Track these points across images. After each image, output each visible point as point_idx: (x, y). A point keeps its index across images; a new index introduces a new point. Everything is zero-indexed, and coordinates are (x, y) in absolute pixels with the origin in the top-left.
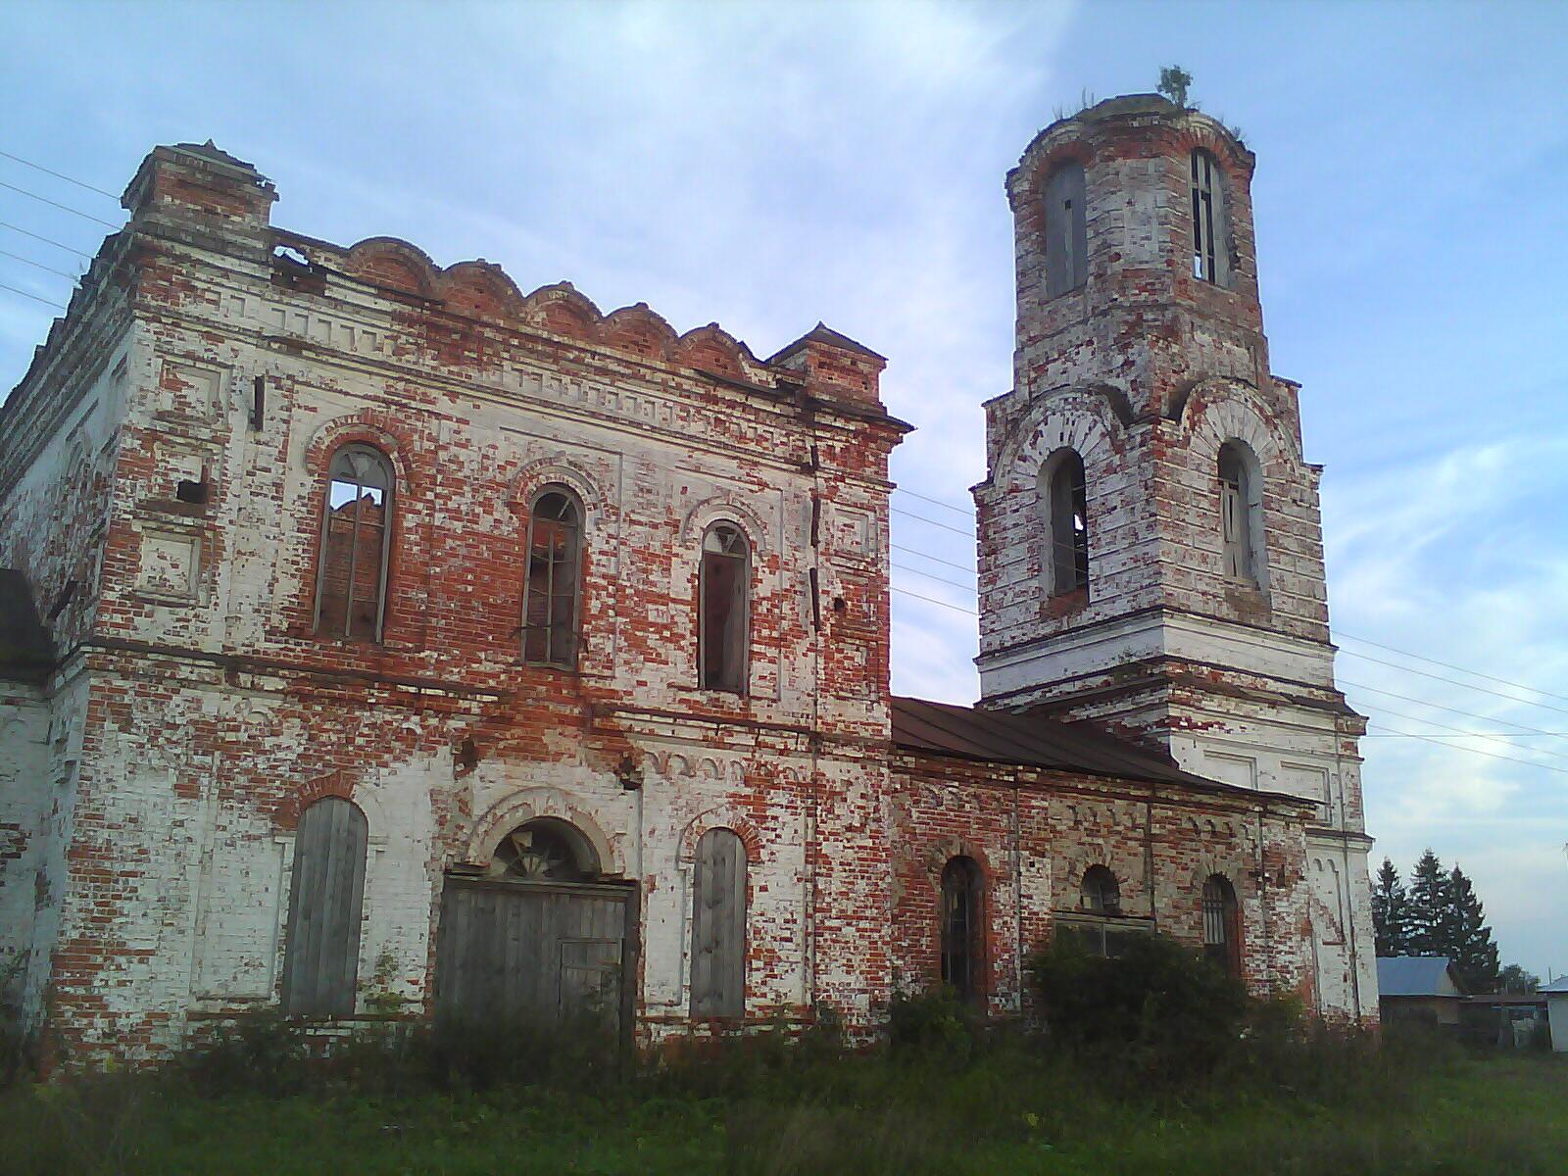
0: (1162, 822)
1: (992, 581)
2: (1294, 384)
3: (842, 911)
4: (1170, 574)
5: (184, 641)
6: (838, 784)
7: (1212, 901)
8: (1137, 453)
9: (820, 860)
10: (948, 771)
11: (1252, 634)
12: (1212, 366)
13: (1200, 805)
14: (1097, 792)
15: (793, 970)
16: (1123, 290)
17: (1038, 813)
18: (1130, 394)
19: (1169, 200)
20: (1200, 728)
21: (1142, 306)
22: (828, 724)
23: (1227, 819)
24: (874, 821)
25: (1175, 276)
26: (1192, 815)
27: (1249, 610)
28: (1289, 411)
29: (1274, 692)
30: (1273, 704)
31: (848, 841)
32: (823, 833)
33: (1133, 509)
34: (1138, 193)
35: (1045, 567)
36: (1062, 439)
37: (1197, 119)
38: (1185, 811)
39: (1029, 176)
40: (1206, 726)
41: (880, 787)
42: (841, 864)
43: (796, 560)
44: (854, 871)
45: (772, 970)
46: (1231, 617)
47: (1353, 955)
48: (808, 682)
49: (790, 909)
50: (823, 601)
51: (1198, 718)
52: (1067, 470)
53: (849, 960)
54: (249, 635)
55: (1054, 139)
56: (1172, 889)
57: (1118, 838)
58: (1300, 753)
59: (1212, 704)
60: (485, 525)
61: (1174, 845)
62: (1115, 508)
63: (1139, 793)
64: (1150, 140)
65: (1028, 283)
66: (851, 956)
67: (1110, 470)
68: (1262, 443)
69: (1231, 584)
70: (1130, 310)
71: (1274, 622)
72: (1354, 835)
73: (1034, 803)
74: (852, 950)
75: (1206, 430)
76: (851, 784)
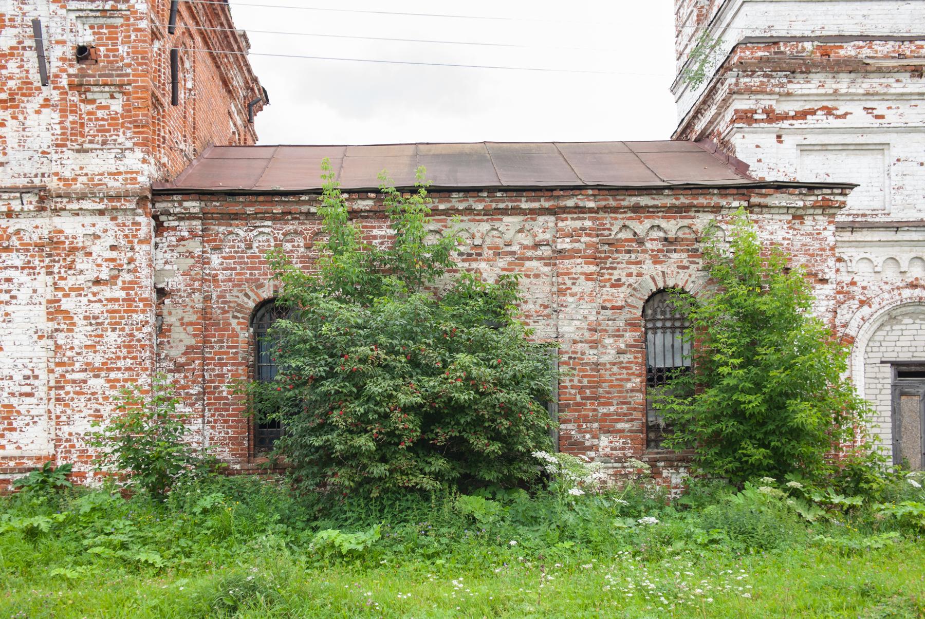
3: (87, 364)
6: (80, 240)
7: (673, 319)
9: (60, 317)
10: (250, 210)
13: (636, 209)
14: (469, 211)
15: (35, 422)
17: (382, 243)
20: (793, 118)
22: (66, 180)
23: (686, 222)
24: (129, 271)
26: (628, 223)
31: (94, 294)
32: (63, 289)
38: (616, 219)
40: (802, 115)
41: (135, 236)
42: (86, 318)
43: (24, 14)
44: (102, 324)
45: (10, 424)
48: (45, 140)
49: (30, 366)
50: (55, 54)
51: (782, 107)
53: (97, 410)
59: (808, 87)
61: (595, 259)
63: (535, 205)
66: (99, 407)
73: (376, 232)
74: (101, 400)
76: (99, 237)
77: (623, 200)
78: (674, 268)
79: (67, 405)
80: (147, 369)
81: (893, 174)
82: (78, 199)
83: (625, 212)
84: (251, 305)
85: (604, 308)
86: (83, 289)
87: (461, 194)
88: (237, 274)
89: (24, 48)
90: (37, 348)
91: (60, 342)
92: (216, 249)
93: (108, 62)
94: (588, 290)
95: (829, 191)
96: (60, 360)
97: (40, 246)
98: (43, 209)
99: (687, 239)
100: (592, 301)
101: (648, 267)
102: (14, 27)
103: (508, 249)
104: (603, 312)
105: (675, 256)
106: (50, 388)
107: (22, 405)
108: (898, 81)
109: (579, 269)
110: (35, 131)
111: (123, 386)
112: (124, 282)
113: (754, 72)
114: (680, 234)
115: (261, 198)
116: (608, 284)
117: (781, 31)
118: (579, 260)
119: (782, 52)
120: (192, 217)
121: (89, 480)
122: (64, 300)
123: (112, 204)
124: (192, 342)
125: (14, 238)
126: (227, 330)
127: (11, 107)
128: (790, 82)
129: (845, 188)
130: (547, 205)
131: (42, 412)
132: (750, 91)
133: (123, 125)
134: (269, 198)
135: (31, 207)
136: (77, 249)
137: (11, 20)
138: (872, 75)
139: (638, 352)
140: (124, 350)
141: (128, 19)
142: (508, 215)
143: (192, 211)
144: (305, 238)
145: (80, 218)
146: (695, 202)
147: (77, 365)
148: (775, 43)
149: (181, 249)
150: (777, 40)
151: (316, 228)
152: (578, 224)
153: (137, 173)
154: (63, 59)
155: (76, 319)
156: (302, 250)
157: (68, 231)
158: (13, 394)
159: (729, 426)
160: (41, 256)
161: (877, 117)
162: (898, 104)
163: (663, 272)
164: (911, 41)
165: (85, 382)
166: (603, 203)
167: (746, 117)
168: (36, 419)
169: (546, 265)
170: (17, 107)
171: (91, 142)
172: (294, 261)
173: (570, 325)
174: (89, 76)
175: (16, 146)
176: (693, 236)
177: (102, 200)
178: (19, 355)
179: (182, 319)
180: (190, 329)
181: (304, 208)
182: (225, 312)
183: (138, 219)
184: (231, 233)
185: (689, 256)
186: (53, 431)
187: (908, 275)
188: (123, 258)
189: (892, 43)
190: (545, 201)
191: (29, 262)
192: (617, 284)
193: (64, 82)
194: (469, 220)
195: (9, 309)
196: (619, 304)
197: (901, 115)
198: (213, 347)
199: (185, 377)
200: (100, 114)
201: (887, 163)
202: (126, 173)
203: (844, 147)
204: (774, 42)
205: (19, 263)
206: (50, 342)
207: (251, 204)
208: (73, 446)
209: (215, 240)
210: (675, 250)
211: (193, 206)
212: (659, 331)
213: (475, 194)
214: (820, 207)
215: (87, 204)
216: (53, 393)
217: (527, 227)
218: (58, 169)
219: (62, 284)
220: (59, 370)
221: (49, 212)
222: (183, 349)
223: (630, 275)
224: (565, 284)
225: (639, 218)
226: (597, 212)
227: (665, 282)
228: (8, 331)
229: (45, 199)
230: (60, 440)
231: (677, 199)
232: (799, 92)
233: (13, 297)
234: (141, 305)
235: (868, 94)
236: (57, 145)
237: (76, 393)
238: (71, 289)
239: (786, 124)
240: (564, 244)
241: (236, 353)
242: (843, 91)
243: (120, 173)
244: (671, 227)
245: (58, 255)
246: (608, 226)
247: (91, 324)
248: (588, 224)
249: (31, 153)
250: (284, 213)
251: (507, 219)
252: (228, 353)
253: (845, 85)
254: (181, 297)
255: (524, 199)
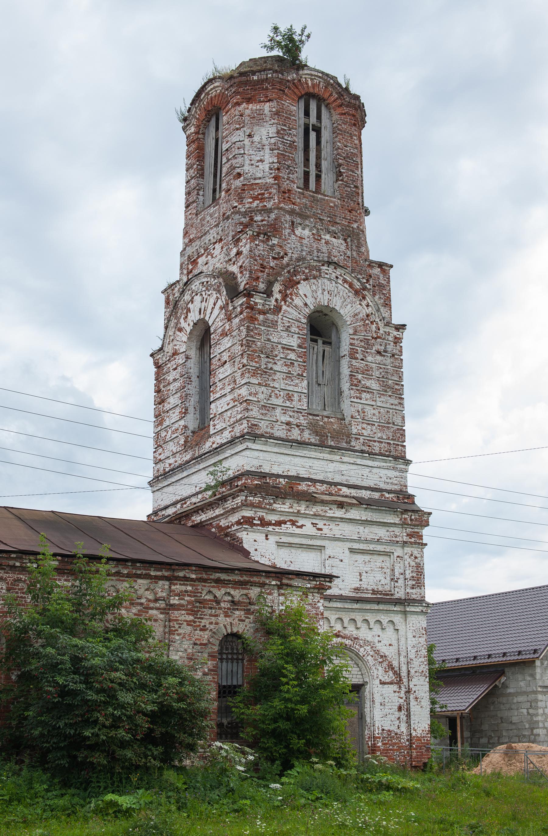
0: (180, 595)
1: (161, 424)
2: (386, 265)
4: (256, 409)
7: (232, 653)
8: (237, 320)
11: (330, 453)
12: (310, 253)
13: (218, 581)
14: (118, 574)
16: (241, 199)
18: (239, 275)
19: (278, 132)
20: (274, 525)
21: (254, 211)
23: (245, 591)
25: (279, 187)
26: (211, 589)
27: (331, 437)
28: (381, 286)
29: (346, 496)
30: (341, 505)
33: (234, 362)
34: (256, 128)
35: (191, 410)
36: (200, 314)
37: (308, 72)
38: (205, 586)
39: (194, 121)
40: (279, 523)
46: (313, 441)
47: (408, 692)
52: (203, 336)
55: (208, 94)
56: (187, 644)
57: (139, 608)
58: (371, 541)
59: (284, 507)
61: (193, 612)
62: (226, 362)
63: (159, 573)
64: (267, 89)
65: (191, 200)
67: (224, 334)
68: (347, 308)
69: (318, 416)
70: (244, 214)
71: (353, 444)
72: (414, 601)
75: (298, 301)
77: (211, 575)
78: (236, 620)
81: (327, 565)
83: (211, 583)
85: (195, 644)
87: (115, 562)
94: (188, 632)
95: (323, 579)
99: (244, 602)
100: (190, 639)
101: (221, 618)
103: (139, 601)
104: (195, 647)
105: (237, 613)
108: (330, 509)
109: (182, 618)
113: (256, 494)
114: (241, 599)
116: (198, 629)
117: (266, 469)
118: (184, 612)
119: (268, 483)
128: (274, 503)
129: (330, 577)
130: (166, 574)
132: (252, 505)
138: (317, 504)
139: (215, 674)
142: (141, 578)
144: (8, 583)
146: (252, 580)
148: (265, 477)
150: (265, 475)
152: (183, 588)
156: (4, 591)
159: (283, 725)
161: (319, 529)
162: (329, 523)
163: (231, 623)
164: (335, 486)
166: (200, 576)
167: (248, 521)
169: (161, 613)
173: (176, 654)
176: (248, 601)
181: (11, 563)
185: (245, 614)
187: (334, 629)
189: (325, 485)
190: (166, 571)
192: (204, 629)
194: (117, 580)
196: (205, 642)
197: (331, 529)
201: (323, 557)
203: (301, 546)
204: (263, 476)
210: (237, 609)
212: (224, 661)
213: (124, 563)
214: (317, 588)
217: (152, 587)
223: (211, 623)
224: (174, 627)
225: (218, 587)
226: (195, 581)
227: (232, 629)
231: (242, 577)
232: (279, 510)
235: (315, 515)
239: (270, 528)
240: (175, 601)
242: (302, 512)
244: (237, 594)
246: (200, 591)
248: (189, 588)
251: (140, 581)
253: (303, 509)
255: (152, 569)
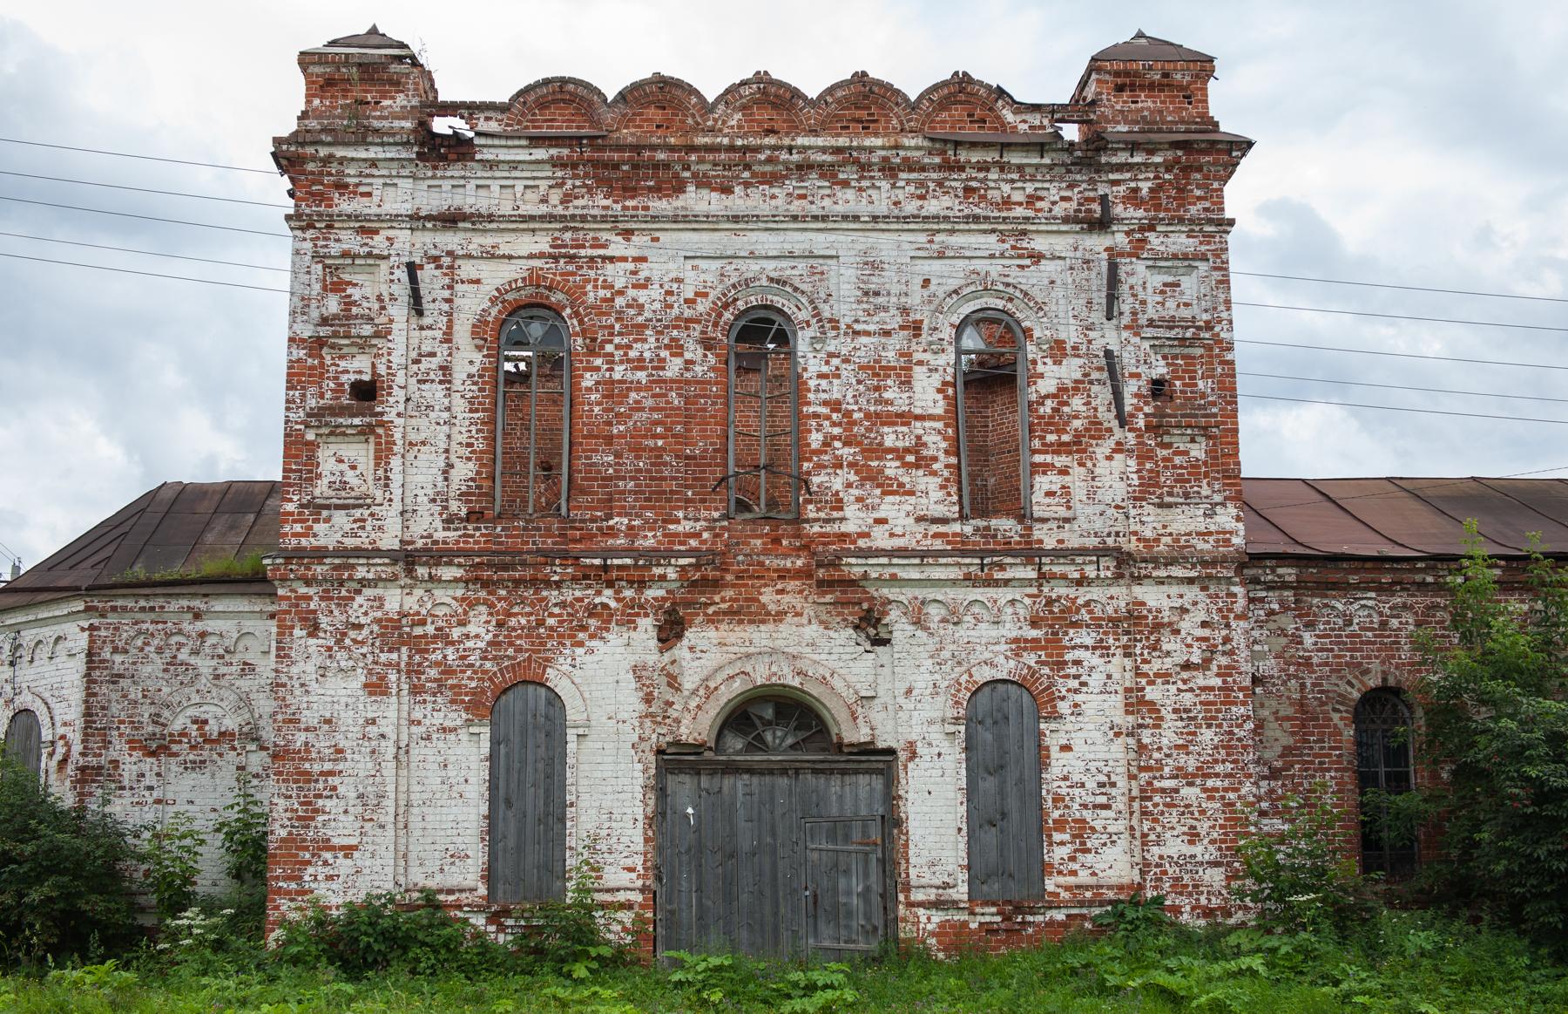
3: (1179, 769)
5: (362, 541)
10: (1353, 579)
24: (1224, 653)
31: (1185, 682)
32: (1146, 675)
41: (1230, 610)
43: (1090, 342)
44: (1195, 718)
45: (1083, 843)
48: (1119, 491)
49: (1105, 770)
50: (1130, 388)
54: (427, 526)
60: (674, 367)
76: (1187, 611)
79: (1156, 821)
80: (1250, 776)
82: (1166, 565)
84: (1356, 695)
86: (1170, 675)
88: (1335, 657)
89: (1091, 382)
90: (1114, 748)
91: (1145, 741)
92: (1310, 625)
93: (1186, 399)
96: (1143, 759)
97: (1115, 621)
98: (1121, 576)
102: (1078, 356)
106: (1132, 799)
107: (1098, 820)
110: (1107, 481)
111: (1223, 798)
112: (1219, 667)
115: (1369, 565)
120: (1284, 586)
121: (1185, 916)
122: (1148, 689)
123: (1207, 570)
124: (1290, 741)
125: (1083, 611)
126: (1328, 726)
127: (1077, 451)
131: (1122, 829)
133: (1206, 475)
134: (1379, 565)
135: (1109, 574)
136: (1162, 625)
137: (1074, 348)
140: (1223, 752)
141: (1211, 349)
143: (1287, 578)
144: (1416, 613)
145: (1165, 588)
147: (1167, 770)
149: (1272, 625)
151: (1428, 601)
153: (1231, 533)
154: (1136, 395)
155: (1164, 712)
157: (1151, 603)
158: (1085, 806)
160: (1115, 633)
165: (1176, 791)
168: (1115, 838)
170: (1085, 451)
171: (1170, 494)
172: (1403, 641)
174: (1170, 416)
175: (1084, 498)
177: (1194, 566)
178: (1092, 756)
179: (1277, 712)
180: (1287, 725)
181: (1418, 578)
182: (1323, 704)
183: (1235, 589)
184: (1326, 605)
186: (1137, 851)
188: (1218, 635)
191: (1101, 640)
193: (1141, 422)
195: (1079, 698)
198: (1311, 748)
199: (1284, 785)
200: (1178, 460)
202: (1218, 533)
205: (1089, 641)
206: (1131, 741)
207: (1356, 571)
208: (1165, 873)
209: (1308, 615)
211: (1289, 573)
215: (1177, 571)
216: (1136, 805)
218: (1138, 528)
219: (1145, 668)
220: (1145, 776)
221: (1126, 581)
222: (1279, 750)
228: (1077, 726)
229: (1127, 564)
230: (1149, 865)
233: (1083, 684)
234: (1241, 695)
236: (1135, 499)
237: (1166, 805)
238: (1157, 675)
241: (1340, 756)
243: (1210, 534)
245: (1140, 632)
247: (1182, 719)
249: (1102, 507)
250: (1394, 583)
252: (1329, 756)
254: (1274, 685)
